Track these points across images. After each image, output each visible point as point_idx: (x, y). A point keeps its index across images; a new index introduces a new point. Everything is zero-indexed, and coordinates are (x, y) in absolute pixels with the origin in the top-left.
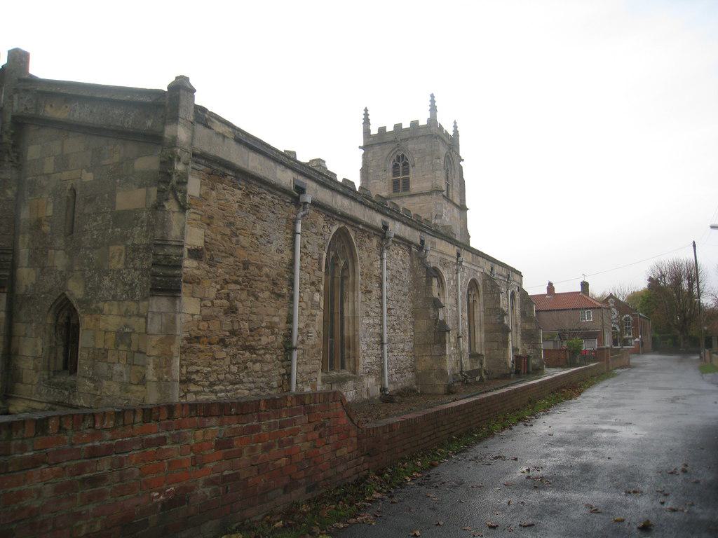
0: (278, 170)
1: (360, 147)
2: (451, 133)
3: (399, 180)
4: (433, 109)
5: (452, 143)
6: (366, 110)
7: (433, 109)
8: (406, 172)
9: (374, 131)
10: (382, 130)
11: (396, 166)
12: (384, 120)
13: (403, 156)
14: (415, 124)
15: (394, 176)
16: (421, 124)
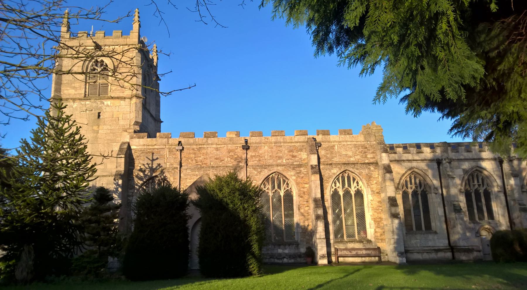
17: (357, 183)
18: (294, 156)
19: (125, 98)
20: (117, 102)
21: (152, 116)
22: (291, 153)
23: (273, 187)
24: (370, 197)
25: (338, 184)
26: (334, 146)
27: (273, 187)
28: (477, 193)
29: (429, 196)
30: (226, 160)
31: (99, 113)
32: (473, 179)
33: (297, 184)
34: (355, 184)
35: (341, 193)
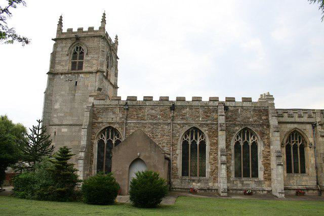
0: (105, 120)
1: (53, 39)
2: (113, 40)
3: (76, 62)
4: (104, 21)
5: (111, 48)
6: (61, 17)
7: (104, 21)
8: (82, 58)
9: (65, 30)
10: (70, 30)
11: (75, 53)
12: (72, 24)
13: (81, 48)
14: (91, 29)
15: (73, 59)
16: (95, 29)
17: (254, 137)
18: (207, 116)
19: (91, 73)
20: (88, 76)
21: (111, 84)
22: (206, 114)
23: (192, 138)
24: (263, 148)
25: (239, 138)
26: (238, 109)
27: (192, 138)
28: (295, 147)
29: (305, 149)
30: (158, 117)
31: (76, 82)
32: (293, 136)
33: (209, 136)
34: (252, 138)
35: (242, 144)
